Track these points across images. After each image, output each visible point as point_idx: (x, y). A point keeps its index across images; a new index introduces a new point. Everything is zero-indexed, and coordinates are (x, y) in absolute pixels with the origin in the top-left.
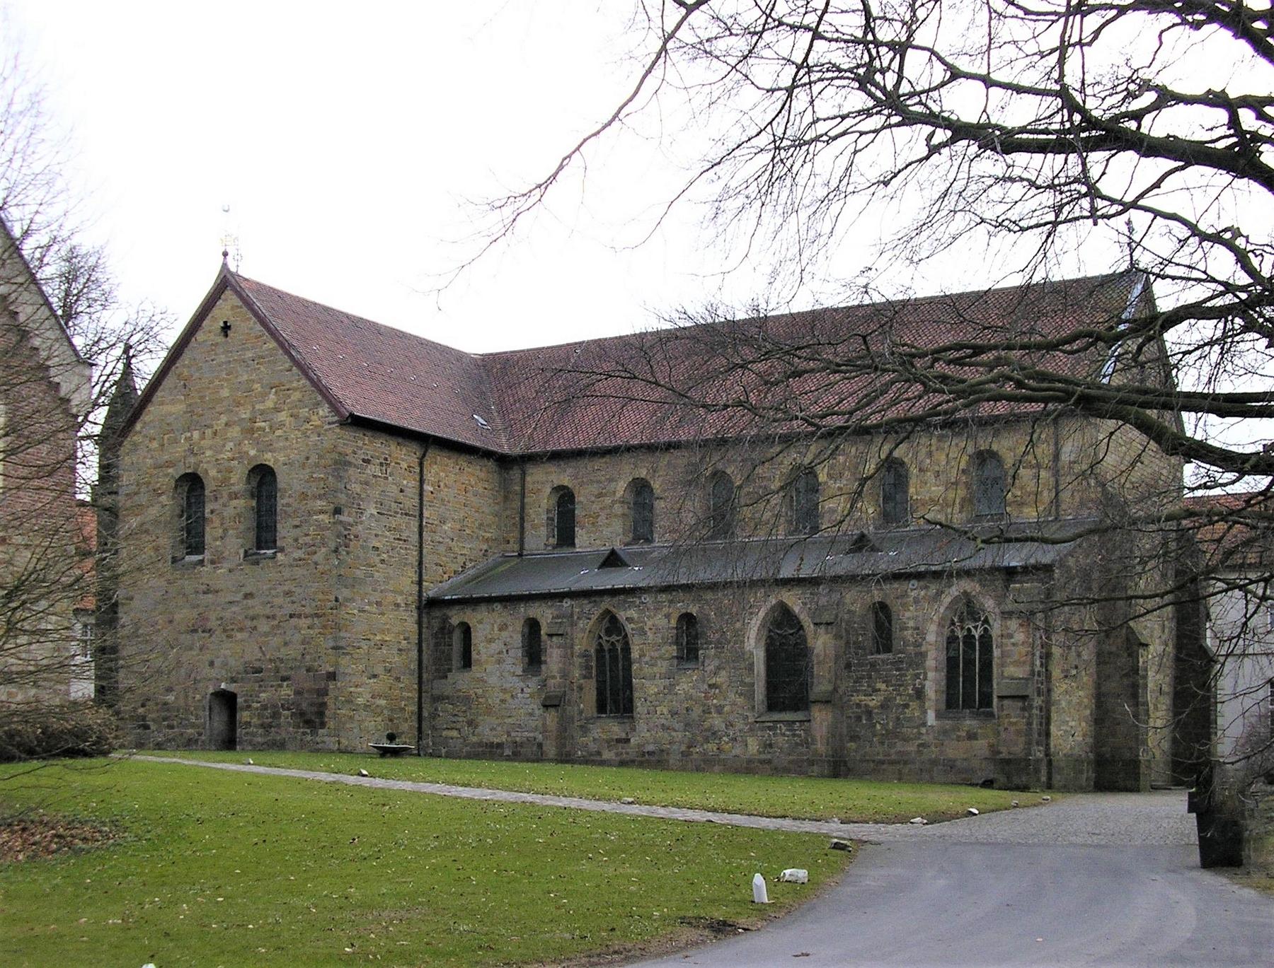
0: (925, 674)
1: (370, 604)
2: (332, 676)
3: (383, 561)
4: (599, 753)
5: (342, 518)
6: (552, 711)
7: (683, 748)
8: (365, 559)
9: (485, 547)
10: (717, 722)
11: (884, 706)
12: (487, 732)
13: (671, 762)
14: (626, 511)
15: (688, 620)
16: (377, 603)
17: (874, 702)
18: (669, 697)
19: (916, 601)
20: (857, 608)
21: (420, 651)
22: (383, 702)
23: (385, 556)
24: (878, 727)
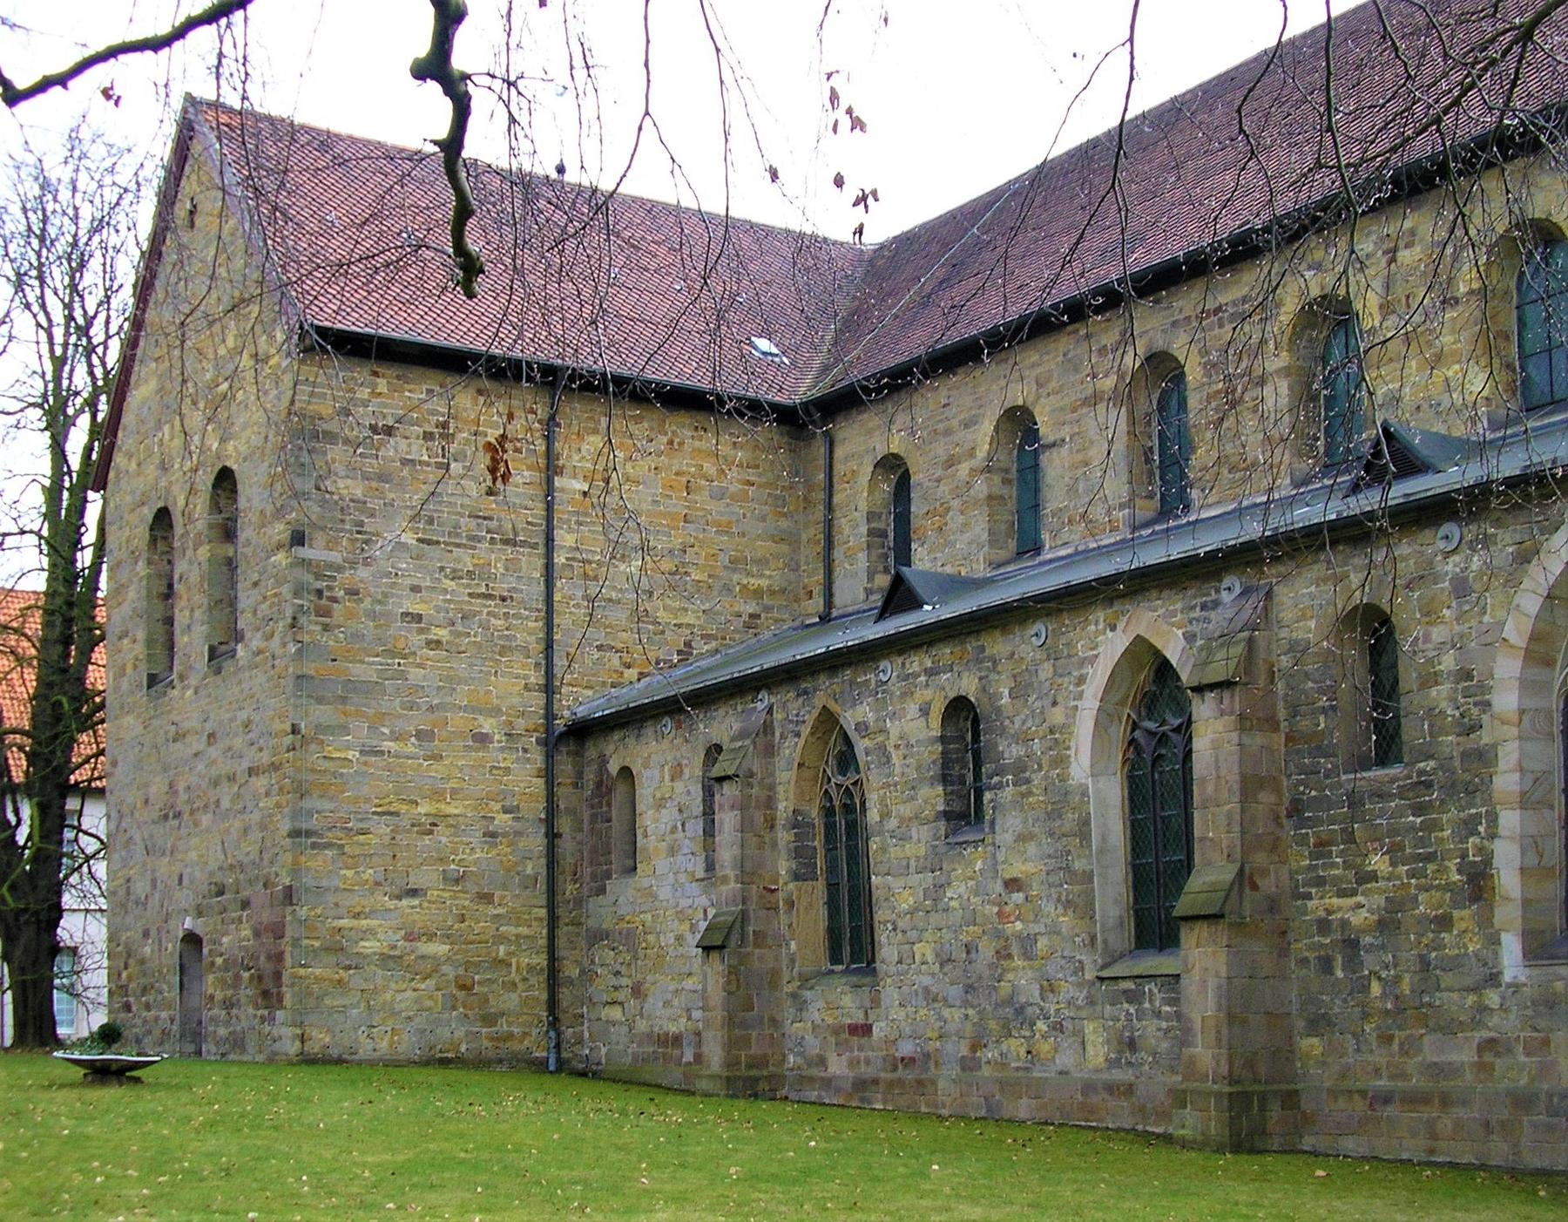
0: (1493, 818)
1: (396, 737)
2: (289, 895)
3: (435, 644)
4: (822, 1062)
5: (304, 552)
6: (715, 955)
7: (964, 1051)
8: (379, 640)
9: (751, 608)
10: (1022, 979)
11: (1387, 924)
12: (660, 1011)
13: (941, 1084)
14: (998, 488)
15: (959, 708)
16: (419, 735)
17: (1359, 911)
18: (935, 918)
19: (1461, 588)
20: (1309, 630)
21: (552, 836)
22: (439, 949)
23: (443, 633)
24: (1376, 988)
